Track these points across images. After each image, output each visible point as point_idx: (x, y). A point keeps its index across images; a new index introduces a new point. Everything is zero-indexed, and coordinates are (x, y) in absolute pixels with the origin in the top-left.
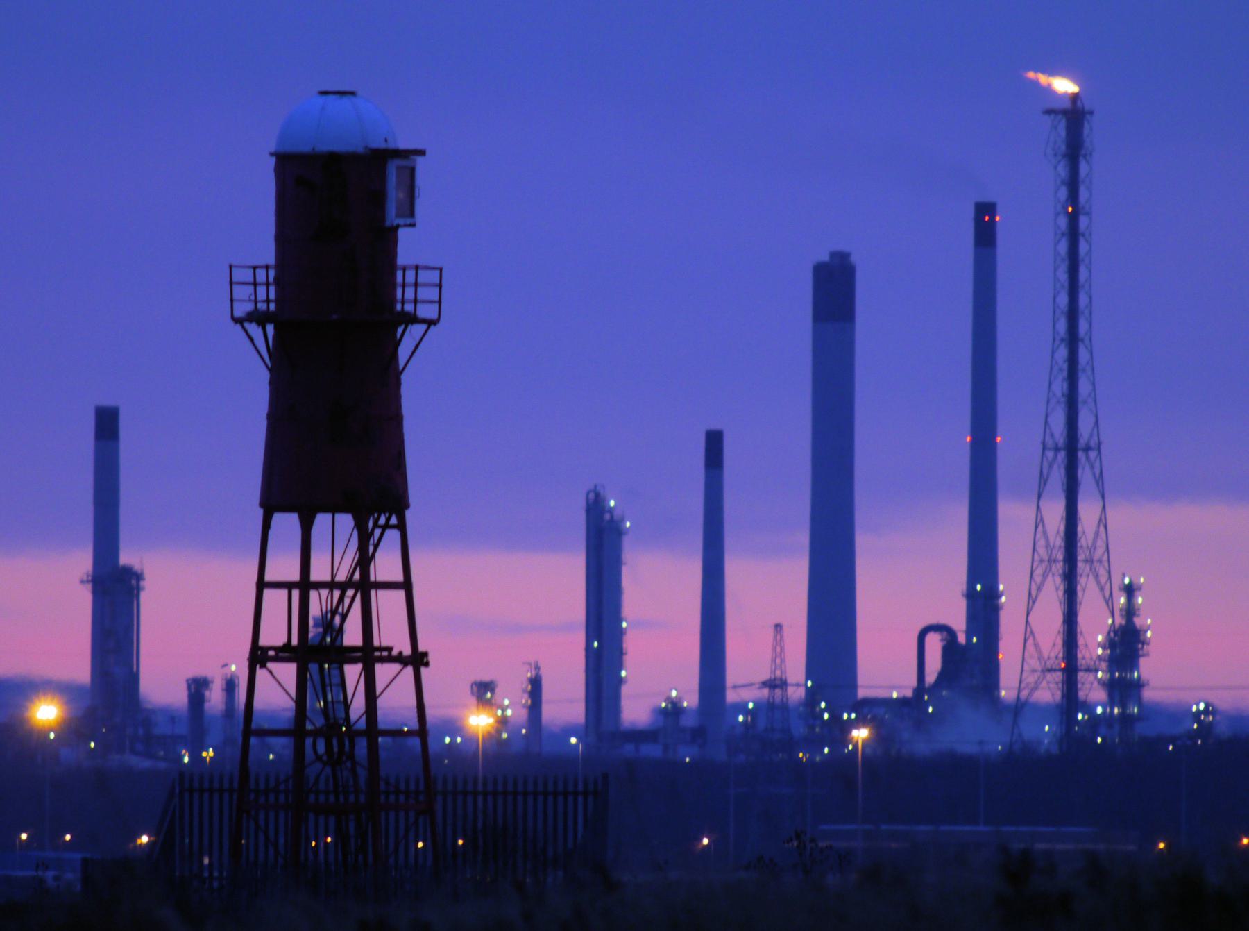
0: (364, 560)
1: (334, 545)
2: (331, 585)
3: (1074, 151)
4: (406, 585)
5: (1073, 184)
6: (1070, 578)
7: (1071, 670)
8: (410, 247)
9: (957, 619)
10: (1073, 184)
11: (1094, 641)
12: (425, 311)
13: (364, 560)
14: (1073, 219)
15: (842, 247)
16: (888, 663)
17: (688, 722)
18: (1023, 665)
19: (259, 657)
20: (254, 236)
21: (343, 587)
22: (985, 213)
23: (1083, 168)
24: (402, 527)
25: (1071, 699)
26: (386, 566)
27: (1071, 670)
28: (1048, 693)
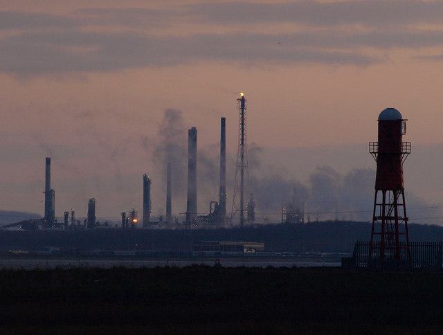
0: (396, 199)
1: (390, 194)
2: (389, 205)
3: (243, 107)
4: (375, 204)
5: (243, 114)
6: (242, 194)
7: (242, 211)
8: (404, 138)
9: (218, 201)
10: (243, 114)
11: (246, 205)
12: (408, 151)
13: (396, 199)
14: (243, 121)
15: (194, 126)
16: (203, 209)
17: (164, 220)
18: (231, 208)
19: (375, 218)
20: (374, 136)
21: (391, 205)
22: (223, 120)
23: (245, 111)
24: (403, 193)
25: (242, 220)
26: (400, 201)
27: (242, 211)
28: (238, 215)
